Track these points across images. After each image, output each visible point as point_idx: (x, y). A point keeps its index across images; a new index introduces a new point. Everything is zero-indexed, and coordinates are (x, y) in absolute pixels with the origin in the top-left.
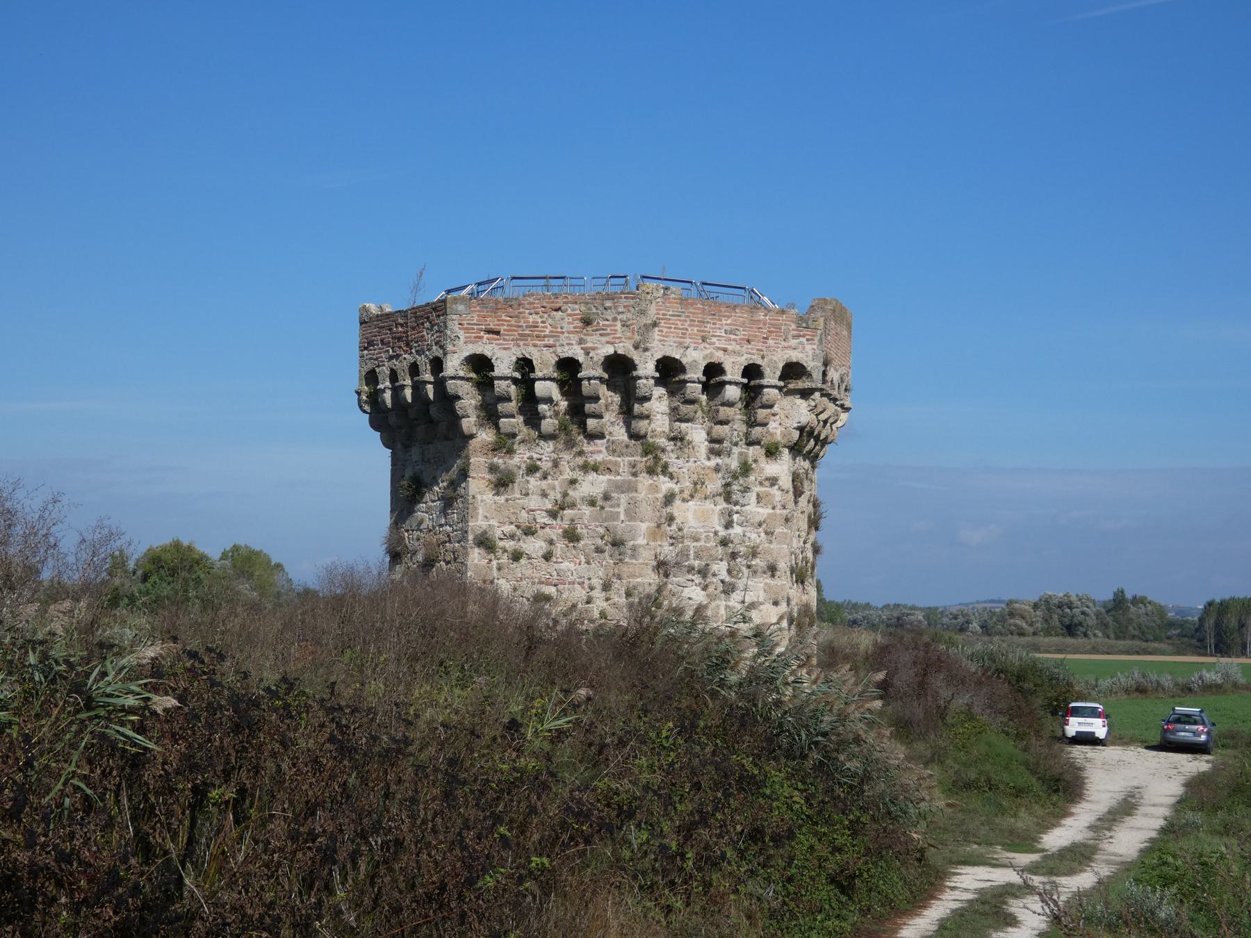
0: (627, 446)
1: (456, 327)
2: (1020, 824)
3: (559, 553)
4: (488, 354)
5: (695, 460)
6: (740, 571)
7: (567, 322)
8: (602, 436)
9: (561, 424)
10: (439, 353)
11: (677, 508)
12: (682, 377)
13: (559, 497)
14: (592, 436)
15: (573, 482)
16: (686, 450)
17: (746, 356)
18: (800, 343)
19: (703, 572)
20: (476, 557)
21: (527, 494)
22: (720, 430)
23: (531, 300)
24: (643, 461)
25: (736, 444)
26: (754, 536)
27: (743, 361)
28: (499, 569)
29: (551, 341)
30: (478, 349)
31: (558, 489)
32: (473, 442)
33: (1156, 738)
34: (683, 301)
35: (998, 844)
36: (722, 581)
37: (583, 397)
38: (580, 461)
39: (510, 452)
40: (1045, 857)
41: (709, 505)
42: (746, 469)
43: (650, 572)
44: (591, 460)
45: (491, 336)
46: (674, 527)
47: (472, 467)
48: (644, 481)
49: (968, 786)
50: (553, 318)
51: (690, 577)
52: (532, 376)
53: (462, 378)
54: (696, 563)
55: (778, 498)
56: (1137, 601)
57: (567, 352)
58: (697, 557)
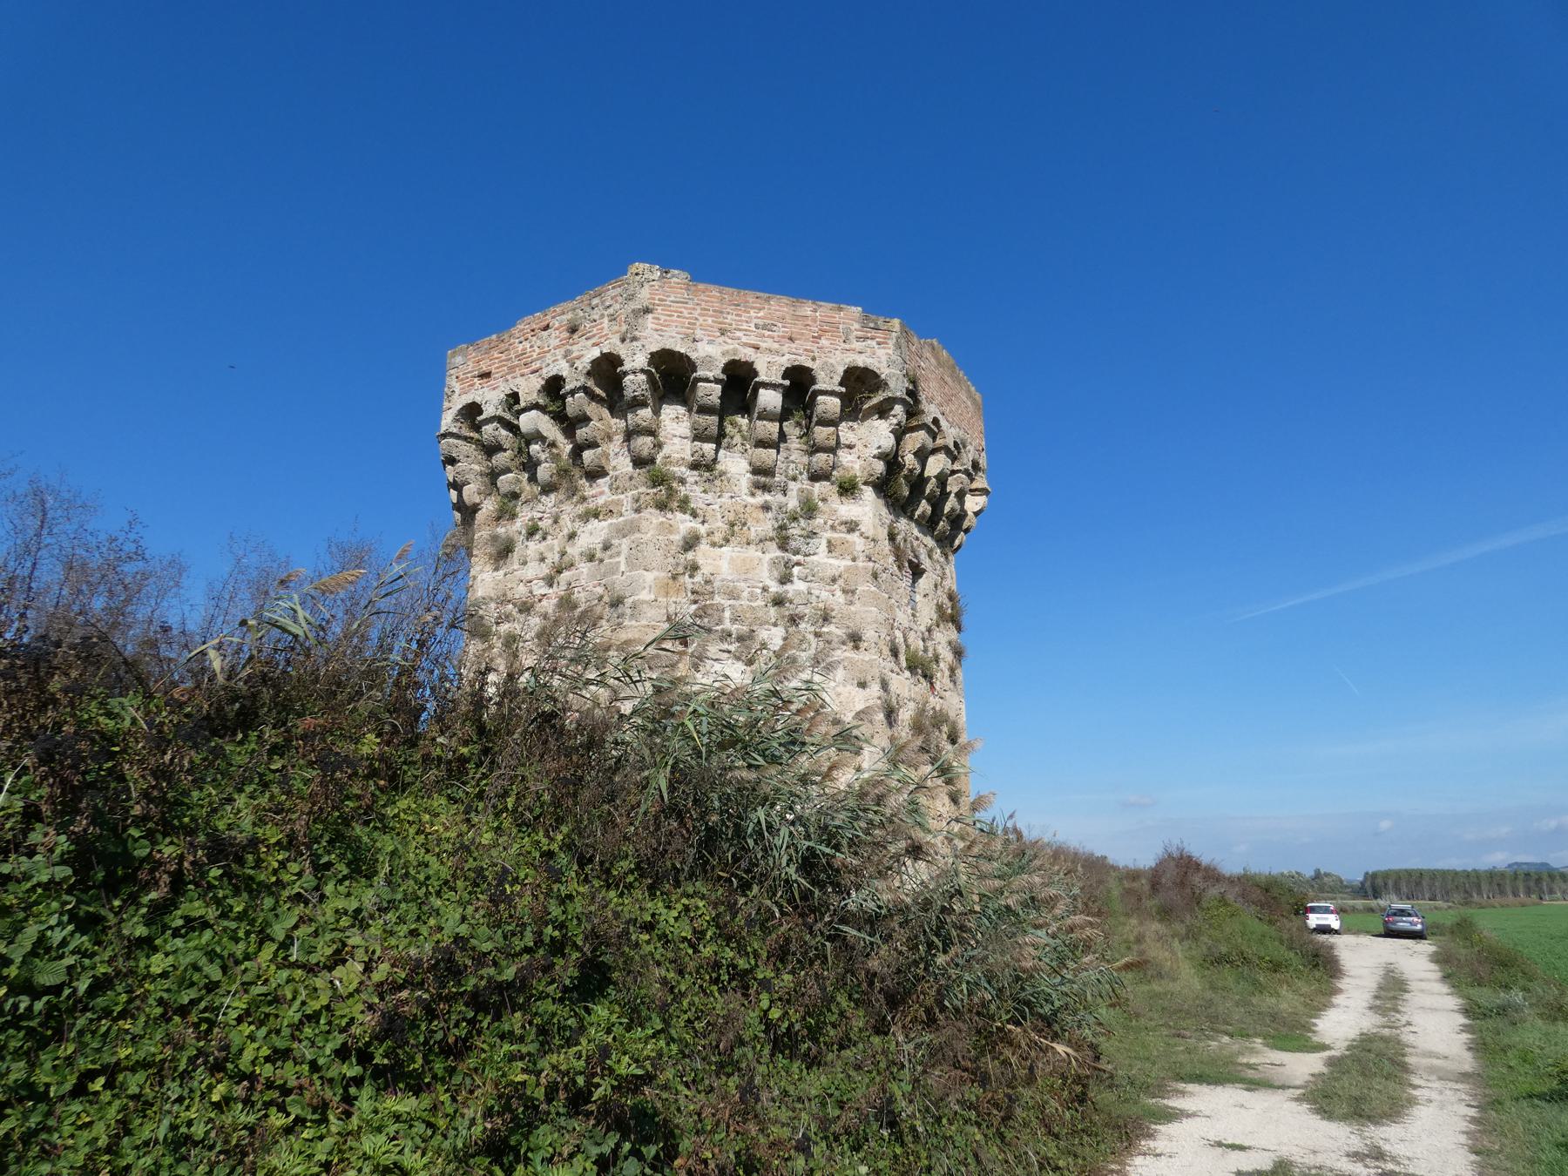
2: (1284, 1006)
11: (703, 555)
16: (717, 482)
17: (788, 356)
25: (794, 479)
26: (824, 595)
33: (1381, 930)
35: (1257, 1035)
38: (581, 509)
40: (1331, 1062)
41: (753, 552)
42: (809, 509)
46: (698, 578)
48: (653, 517)
49: (1220, 960)
51: (725, 646)
56: (1327, 875)
58: (734, 620)
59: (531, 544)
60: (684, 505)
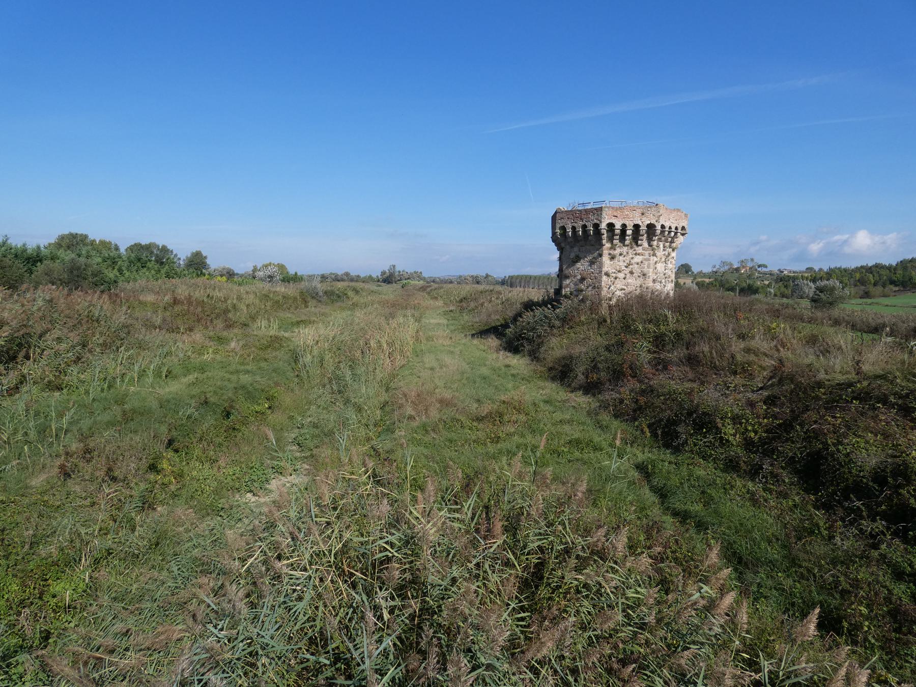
5: (660, 253)
7: (637, 214)
14: (638, 245)
20: (604, 278)
30: (611, 221)
37: (636, 235)
42: (669, 254)
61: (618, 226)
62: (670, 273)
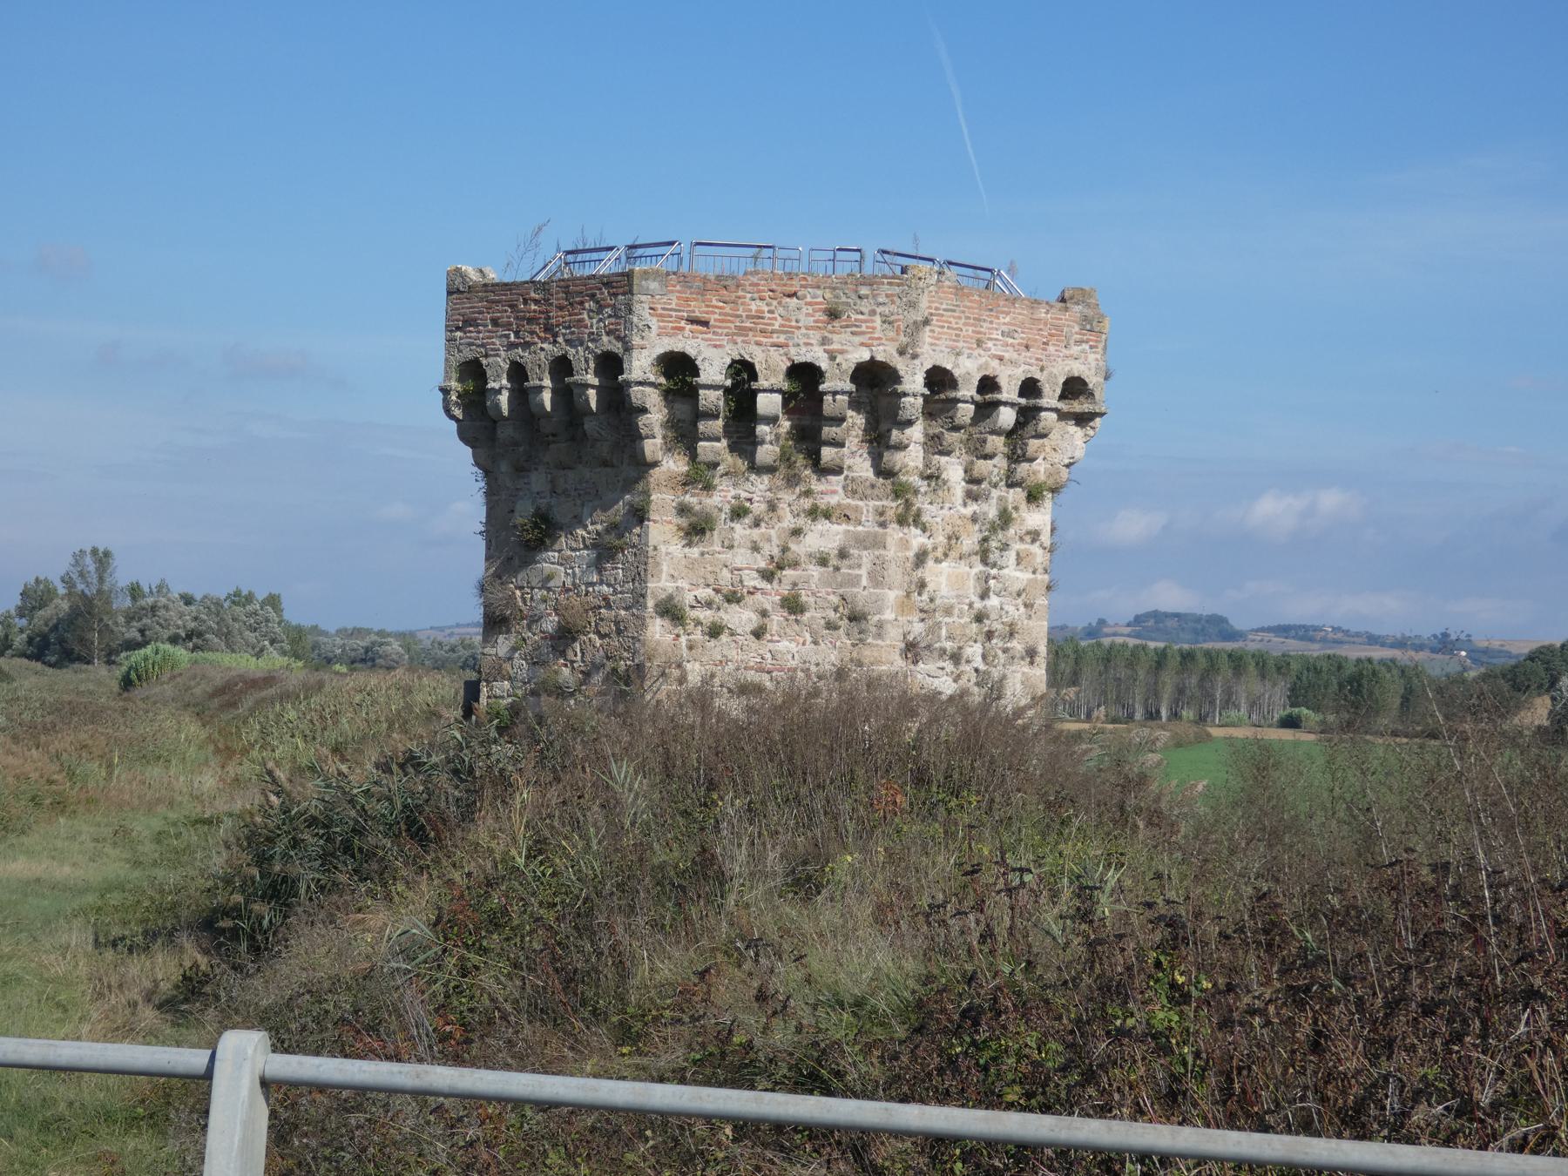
0: (873, 486)
1: (646, 313)
3: (775, 628)
4: (691, 352)
5: (948, 509)
6: (995, 656)
7: (806, 313)
8: (838, 471)
9: (783, 453)
10: (617, 347)
12: (952, 394)
13: (776, 552)
14: (823, 471)
15: (797, 532)
17: (1023, 367)
18: (1083, 351)
19: (956, 658)
20: (657, 631)
21: (731, 547)
22: (982, 466)
23: (755, 280)
24: (893, 506)
25: (995, 486)
26: (1011, 609)
27: (1020, 373)
28: (691, 648)
29: (782, 339)
31: (775, 541)
32: (656, 473)
34: (959, 290)
36: (977, 670)
37: (808, 417)
38: (807, 503)
39: (708, 487)
41: (963, 568)
42: (1005, 519)
43: (897, 657)
44: (823, 502)
45: (695, 327)
46: (925, 597)
47: (653, 507)
48: (894, 533)
50: (786, 307)
51: (941, 664)
52: (754, 385)
53: (652, 384)
54: (948, 645)
55: (1039, 559)
57: (802, 356)
58: (950, 637)
59: (737, 526)
60: (917, 521)
61: (713, 371)
62: (1015, 611)
